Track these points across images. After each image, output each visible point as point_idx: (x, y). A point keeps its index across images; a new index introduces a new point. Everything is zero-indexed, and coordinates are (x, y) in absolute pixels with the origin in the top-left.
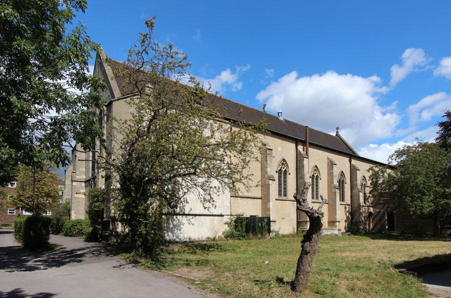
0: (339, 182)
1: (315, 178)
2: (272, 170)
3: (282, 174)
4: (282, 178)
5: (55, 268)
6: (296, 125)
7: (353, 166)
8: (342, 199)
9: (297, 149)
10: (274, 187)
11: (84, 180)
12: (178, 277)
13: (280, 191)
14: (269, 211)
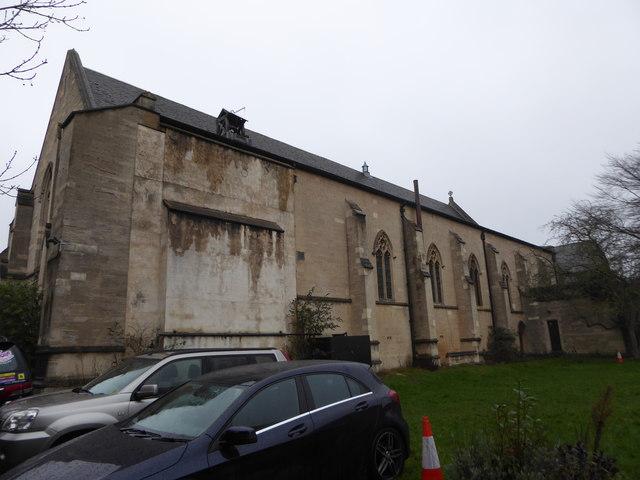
0: (430, 264)
1: (435, 267)
2: (366, 250)
3: (383, 257)
4: (383, 265)
5: (61, 463)
6: (94, 72)
7: (489, 245)
8: (479, 303)
9: (402, 217)
10: (371, 280)
11: (500, 325)
12: (599, 432)
13: (380, 288)
14: (367, 324)
